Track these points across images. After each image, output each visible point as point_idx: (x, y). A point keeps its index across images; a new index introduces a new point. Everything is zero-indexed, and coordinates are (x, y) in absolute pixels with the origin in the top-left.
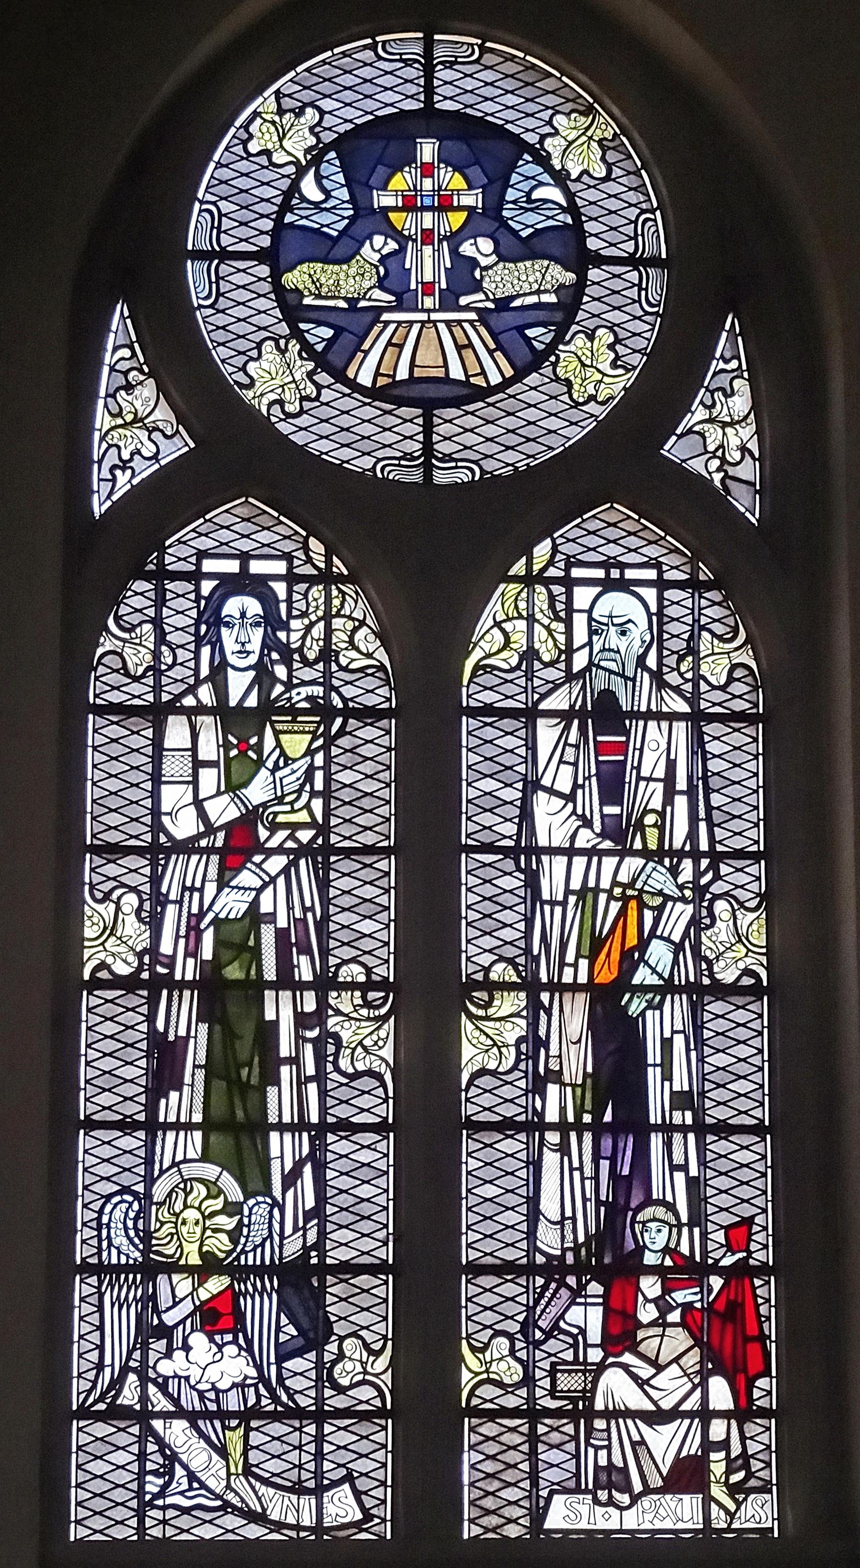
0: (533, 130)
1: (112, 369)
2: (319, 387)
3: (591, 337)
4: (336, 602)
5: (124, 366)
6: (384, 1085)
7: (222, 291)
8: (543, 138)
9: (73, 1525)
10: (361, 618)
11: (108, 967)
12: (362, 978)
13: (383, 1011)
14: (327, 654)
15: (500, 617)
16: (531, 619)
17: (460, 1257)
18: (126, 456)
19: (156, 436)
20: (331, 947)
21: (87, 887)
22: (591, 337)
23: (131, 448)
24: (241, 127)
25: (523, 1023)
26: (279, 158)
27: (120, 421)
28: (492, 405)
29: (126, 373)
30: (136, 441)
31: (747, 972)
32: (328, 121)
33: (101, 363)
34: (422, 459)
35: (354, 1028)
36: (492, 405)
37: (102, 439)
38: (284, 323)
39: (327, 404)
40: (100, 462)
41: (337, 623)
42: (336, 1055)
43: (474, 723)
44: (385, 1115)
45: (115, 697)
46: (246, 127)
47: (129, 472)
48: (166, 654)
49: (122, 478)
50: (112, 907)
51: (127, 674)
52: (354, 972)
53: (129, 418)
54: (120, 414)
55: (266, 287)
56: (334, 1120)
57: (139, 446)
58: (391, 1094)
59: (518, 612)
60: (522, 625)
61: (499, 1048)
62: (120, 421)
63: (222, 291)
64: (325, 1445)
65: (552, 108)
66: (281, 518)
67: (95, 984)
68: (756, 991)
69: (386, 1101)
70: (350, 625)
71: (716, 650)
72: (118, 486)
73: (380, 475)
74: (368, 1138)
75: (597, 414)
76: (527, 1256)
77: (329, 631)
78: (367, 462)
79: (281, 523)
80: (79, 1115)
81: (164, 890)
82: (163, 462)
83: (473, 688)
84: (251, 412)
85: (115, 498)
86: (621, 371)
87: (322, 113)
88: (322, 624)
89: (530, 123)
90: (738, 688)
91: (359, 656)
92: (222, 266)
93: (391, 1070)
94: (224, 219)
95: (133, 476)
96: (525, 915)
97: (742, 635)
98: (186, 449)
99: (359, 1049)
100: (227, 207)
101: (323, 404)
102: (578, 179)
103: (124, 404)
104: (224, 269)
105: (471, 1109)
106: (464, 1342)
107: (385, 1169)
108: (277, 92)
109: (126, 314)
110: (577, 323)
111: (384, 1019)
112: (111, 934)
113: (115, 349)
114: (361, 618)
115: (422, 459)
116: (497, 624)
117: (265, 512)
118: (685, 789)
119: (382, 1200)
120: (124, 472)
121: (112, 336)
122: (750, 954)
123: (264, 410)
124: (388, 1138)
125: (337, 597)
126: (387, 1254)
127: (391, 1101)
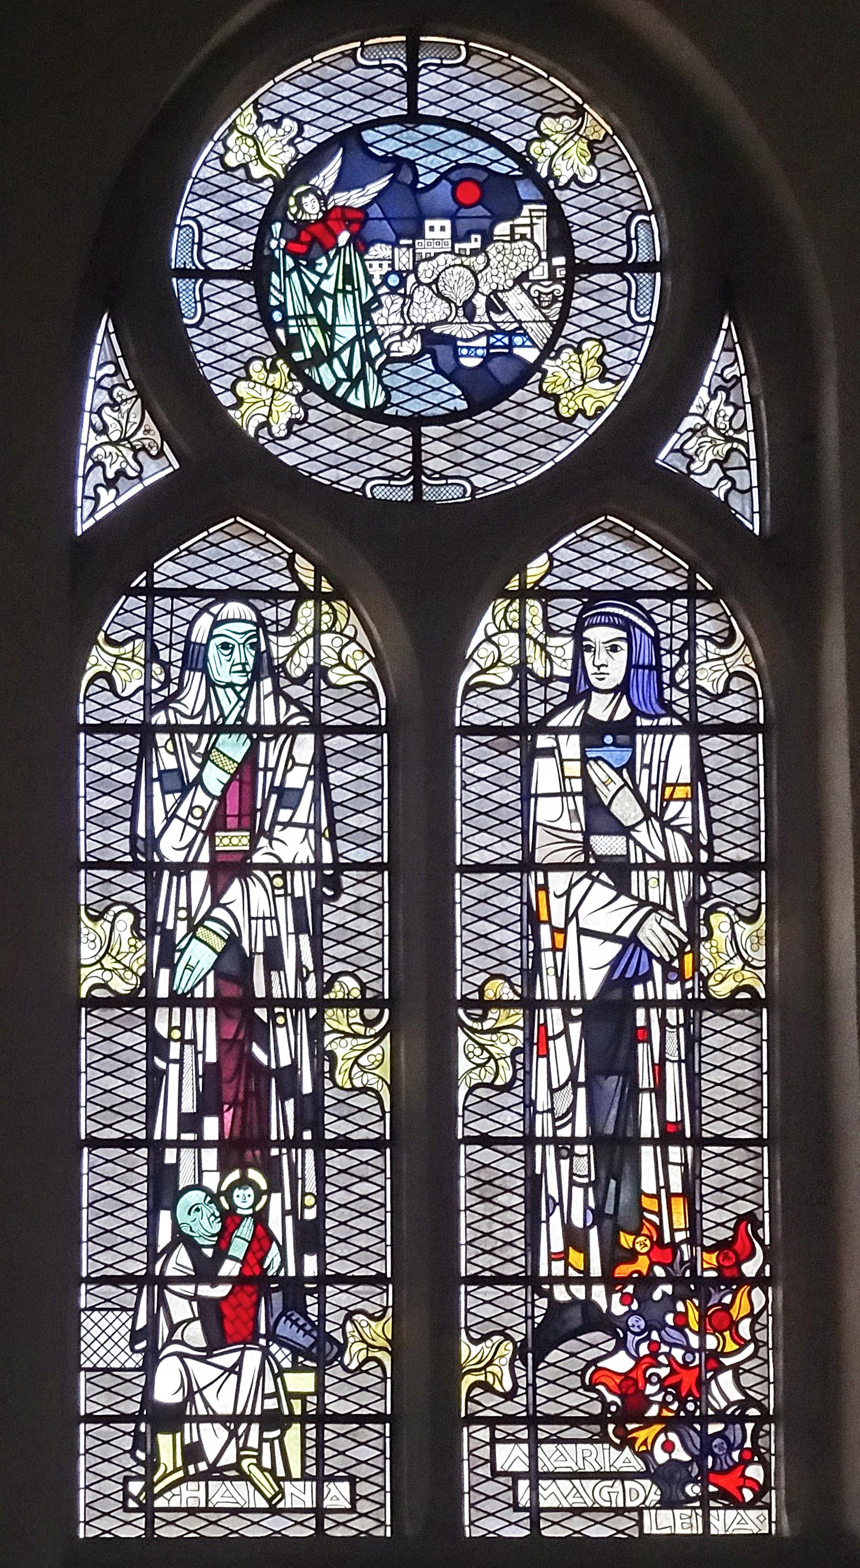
0: (520, 137)
1: (98, 385)
2: (306, 408)
3: (579, 351)
4: (326, 619)
5: (106, 383)
6: (381, 1103)
7: (207, 311)
8: (529, 143)
9: (82, 1525)
10: (352, 635)
11: (105, 986)
12: (356, 994)
13: (378, 1028)
14: (318, 671)
15: (492, 630)
16: (522, 632)
17: (460, 1410)
18: (111, 475)
19: (142, 456)
20: (324, 930)
21: (83, 908)
22: (579, 351)
23: (116, 467)
24: (218, 140)
25: (520, 1034)
26: (258, 171)
27: (104, 439)
28: (481, 422)
29: (110, 391)
30: (121, 459)
31: (749, 989)
32: (309, 131)
33: (87, 377)
34: (411, 478)
35: (350, 1046)
36: (481, 422)
37: (89, 455)
38: (269, 343)
39: (315, 425)
40: (85, 477)
41: (325, 639)
42: (332, 1071)
43: (468, 744)
44: (382, 1132)
45: (106, 716)
46: (223, 140)
47: (113, 492)
48: (158, 671)
49: (107, 496)
50: (107, 926)
51: (116, 694)
52: (349, 986)
53: (115, 437)
54: (104, 430)
55: (251, 307)
56: (334, 1136)
57: (124, 465)
58: (389, 1375)
59: (507, 624)
60: (514, 638)
61: (496, 1061)
62: (104, 439)
63: (207, 311)
64: (326, 1450)
65: (540, 111)
66: (268, 536)
67: (93, 1003)
68: (754, 1003)
69: (384, 1379)
70: (338, 643)
71: (711, 656)
72: (102, 503)
73: (369, 496)
74: (367, 1154)
75: (586, 427)
76: (527, 1410)
77: (317, 648)
78: (356, 483)
79: (268, 541)
80: (79, 1133)
81: (160, 919)
82: (147, 483)
83: (467, 710)
84: (237, 431)
85: (99, 516)
86: (609, 385)
87: (301, 124)
88: (311, 642)
89: (516, 129)
90: (733, 700)
91: (348, 672)
92: (206, 286)
93: (389, 1087)
94: (205, 234)
95: (118, 495)
96: (521, 898)
97: (740, 638)
98: (170, 470)
99: (356, 1069)
100: (212, 373)
101: (310, 425)
102: (567, 186)
103: (109, 421)
104: (208, 289)
105: (466, 884)
106: (463, 1332)
107: (380, 973)
108: (256, 102)
109: (111, 329)
110: (564, 337)
111: (381, 1035)
112: (106, 952)
113: (99, 367)
114: (352, 635)
115: (411, 478)
116: (488, 639)
117: (251, 530)
118: (680, 1191)
119: (376, 778)
120: (108, 490)
121: (97, 348)
122: (747, 968)
123: (251, 433)
124: (387, 1291)
125: (327, 613)
126: (385, 1268)
127: (389, 1381)
